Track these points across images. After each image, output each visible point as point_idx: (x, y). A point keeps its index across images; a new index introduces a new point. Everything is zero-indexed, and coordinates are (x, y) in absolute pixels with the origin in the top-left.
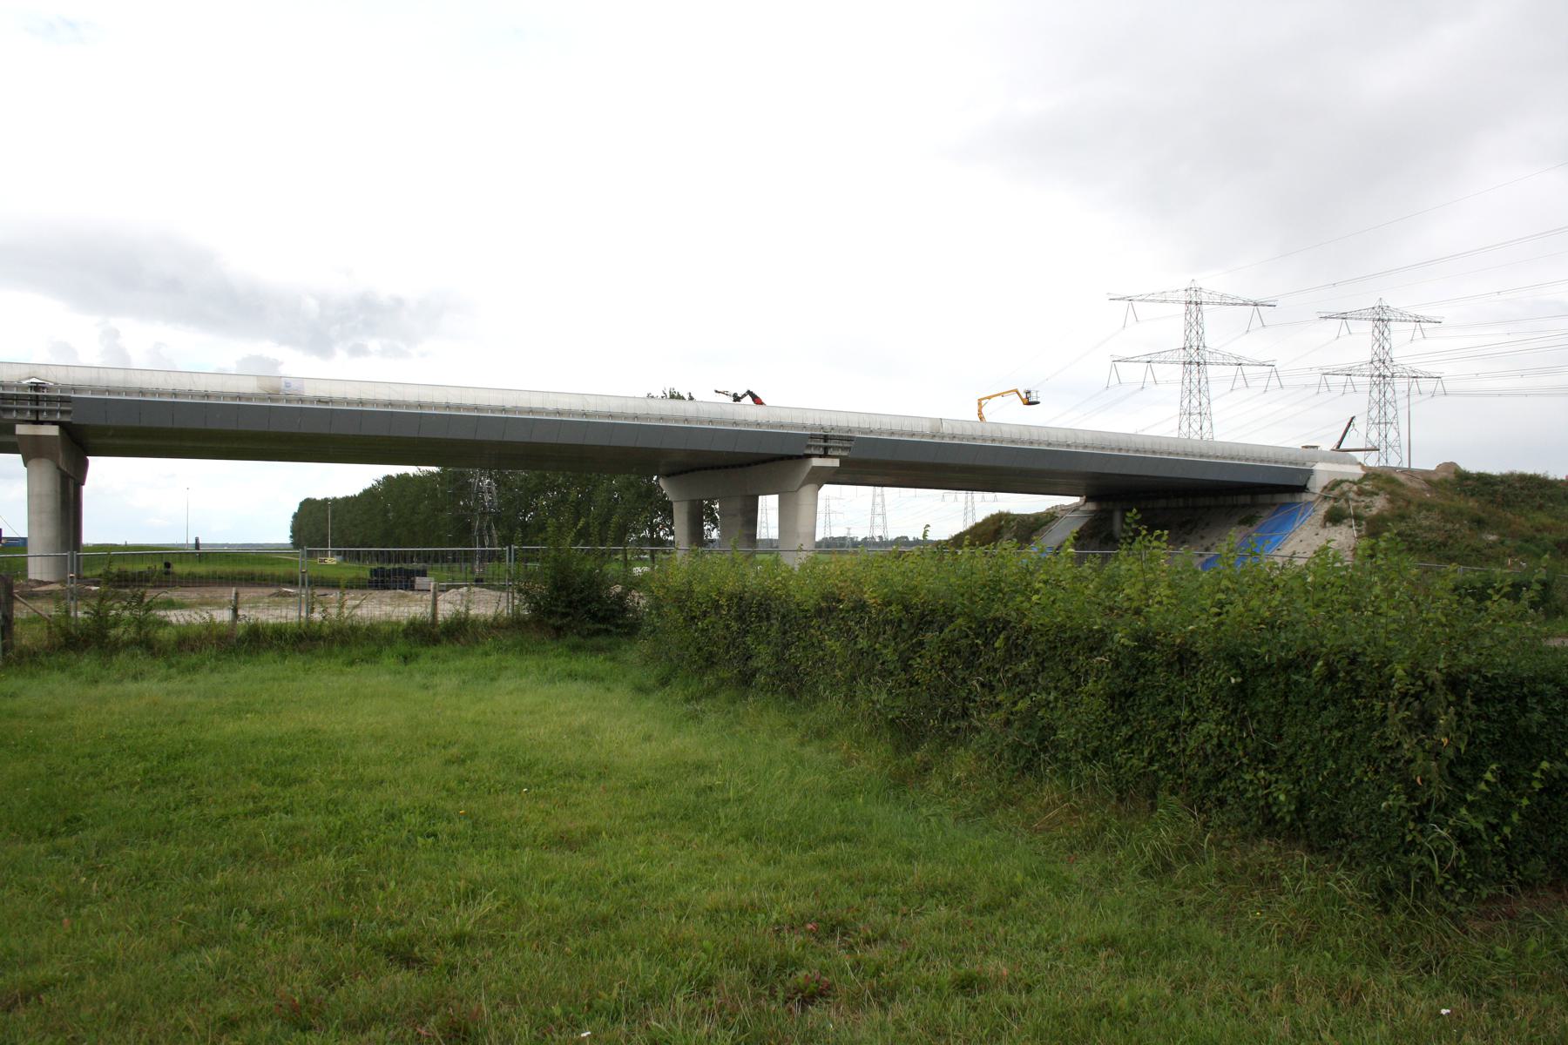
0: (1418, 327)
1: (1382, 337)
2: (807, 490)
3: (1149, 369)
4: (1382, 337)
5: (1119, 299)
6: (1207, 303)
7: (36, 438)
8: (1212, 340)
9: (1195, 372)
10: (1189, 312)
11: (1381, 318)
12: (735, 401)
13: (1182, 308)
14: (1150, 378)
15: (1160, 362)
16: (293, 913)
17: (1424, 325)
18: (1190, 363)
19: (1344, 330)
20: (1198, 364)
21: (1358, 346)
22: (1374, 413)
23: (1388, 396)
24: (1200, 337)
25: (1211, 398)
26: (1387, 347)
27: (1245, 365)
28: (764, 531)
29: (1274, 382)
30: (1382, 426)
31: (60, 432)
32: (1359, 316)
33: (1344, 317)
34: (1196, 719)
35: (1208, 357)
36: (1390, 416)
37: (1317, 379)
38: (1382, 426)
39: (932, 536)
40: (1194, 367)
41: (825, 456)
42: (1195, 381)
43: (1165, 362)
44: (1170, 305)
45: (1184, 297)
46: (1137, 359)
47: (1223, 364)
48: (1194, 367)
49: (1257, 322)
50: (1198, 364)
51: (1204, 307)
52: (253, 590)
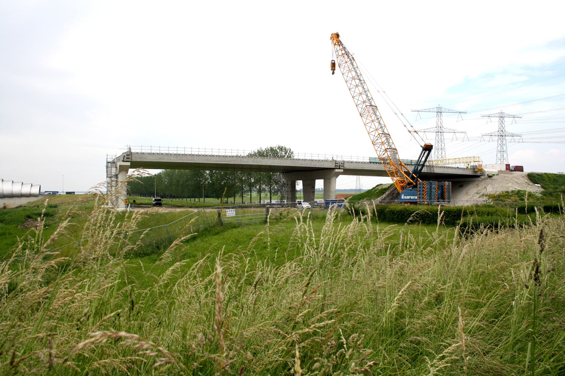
0: (514, 120)
1: (502, 122)
2: (335, 178)
4: (502, 122)
9: (440, 135)
11: (502, 117)
16: (433, 319)
20: (441, 132)
21: (494, 126)
22: (499, 148)
23: (504, 142)
26: (503, 126)
27: (410, 124)
30: (502, 153)
34: (184, 266)
35: (444, 130)
36: (505, 149)
38: (502, 153)
40: (439, 133)
41: (339, 168)
42: (440, 138)
45: (436, 110)
48: (439, 133)
50: (441, 132)
51: (443, 113)
52: (393, 224)
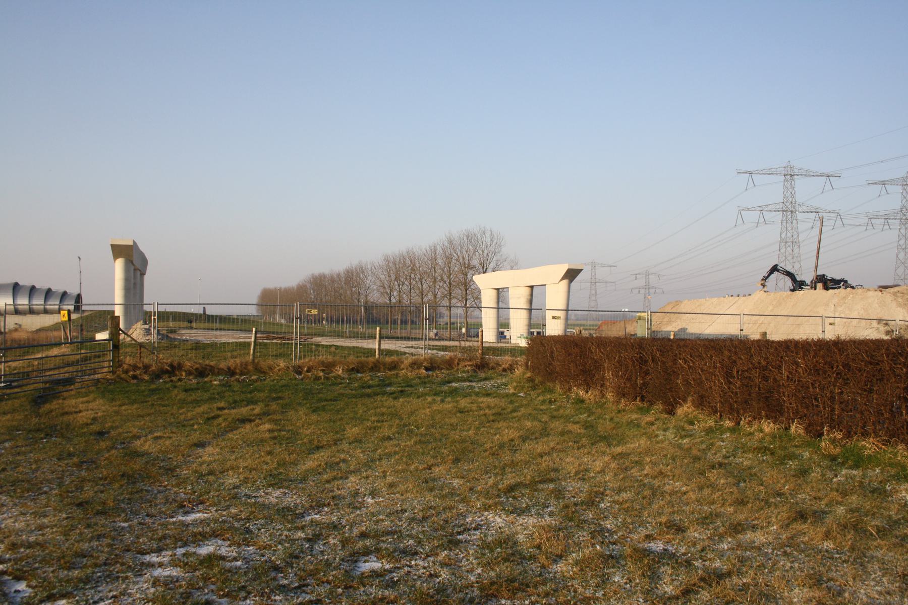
3: (761, 215)
5: (743, 173)
6: (798, 175)
7: (245, 342)
8: (799, 198)
10: (786, 180)
12: (776, 265)
13: (782, 178)
14: (762, 220)
15: (767, 211)
17: (831, 178)
18: (786, 211)
19: (884, 191)
24: (793, 195)
25: (799, 231)
28: (737, 332)
29: (839, 222)
31: (553, 338)
32: (892, 182)
33: (883, 183)
37: (866, 220)
39: (167, 311)
43: (771, 211)
44: (775, 176)
46: (754, 209)
47: (807, 212)
49: (828, 187)
51: (795, 177)
